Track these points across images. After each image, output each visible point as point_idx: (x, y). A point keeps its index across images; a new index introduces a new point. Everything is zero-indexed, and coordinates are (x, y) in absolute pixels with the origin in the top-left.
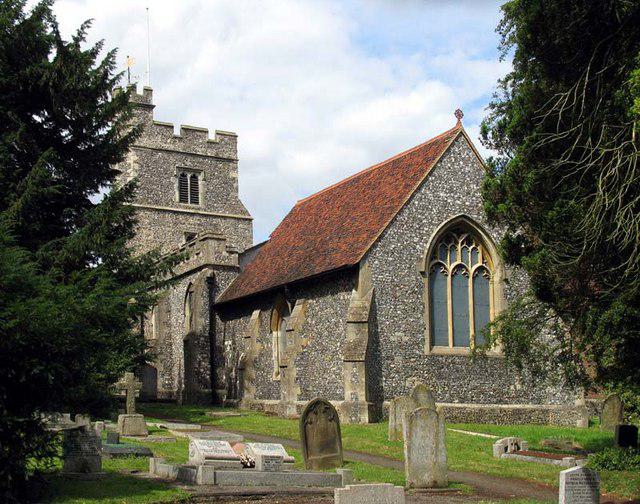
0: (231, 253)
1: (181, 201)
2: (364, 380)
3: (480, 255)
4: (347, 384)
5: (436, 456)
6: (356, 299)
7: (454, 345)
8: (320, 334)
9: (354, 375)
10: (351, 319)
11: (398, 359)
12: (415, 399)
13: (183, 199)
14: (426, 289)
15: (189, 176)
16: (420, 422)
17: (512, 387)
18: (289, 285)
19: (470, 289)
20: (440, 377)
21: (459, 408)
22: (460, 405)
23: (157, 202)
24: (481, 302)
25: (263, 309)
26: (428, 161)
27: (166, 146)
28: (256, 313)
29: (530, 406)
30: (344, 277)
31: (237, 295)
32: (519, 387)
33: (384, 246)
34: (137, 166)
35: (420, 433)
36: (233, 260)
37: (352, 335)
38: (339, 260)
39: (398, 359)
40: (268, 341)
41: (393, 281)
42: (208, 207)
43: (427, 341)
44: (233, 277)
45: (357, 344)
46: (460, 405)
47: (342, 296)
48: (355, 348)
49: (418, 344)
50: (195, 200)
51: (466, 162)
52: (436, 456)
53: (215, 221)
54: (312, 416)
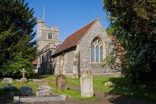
0: (55, 46)
1: (49, 39)
2: (77, 69)
3: (101, 44)
4: (74, 70)
5: (90, 90)
6: (76, 52)
7: (96, 62)
8: (69, 60)
9: (75, 68)
10: (75, 57)
11: (85, 65)
12: (87, 73)
13: (49, 38)
14: (90, 54)
15: (50, 34)
16: (86, 81)
17: (107, 70)
18: (64, 51)
19: (99, 50)
20: (93, 68)
21: (97, 74)
22: (97, 74)
23: (44, 39)
24: (102, 53)
25: (59, 56)
26: (93, 23)
27: (46, 29)
28: (58, 57)
29: (111, 74)
30: (74, 48)
31: (55, 54)
32: (109, 70)
33: (82, 42)
34: (41, 33)
35: (85, 84)
36: (55, 47)
37: (75, 60)
38: (73, 45)
39: (85, 65)
40: (60, 62)
41: (84, 49)
42: (54, 40)
43: (91, 61)
44: (55, 50)
45: (76, 62)
46: (97, 74)
47: (73, 52)
48: (76, 63)
49: (89, 62)
50: (51, 39)
51: (99, 25)
52: (90, 90)
53: (55, 42)
54: (59, 78)
